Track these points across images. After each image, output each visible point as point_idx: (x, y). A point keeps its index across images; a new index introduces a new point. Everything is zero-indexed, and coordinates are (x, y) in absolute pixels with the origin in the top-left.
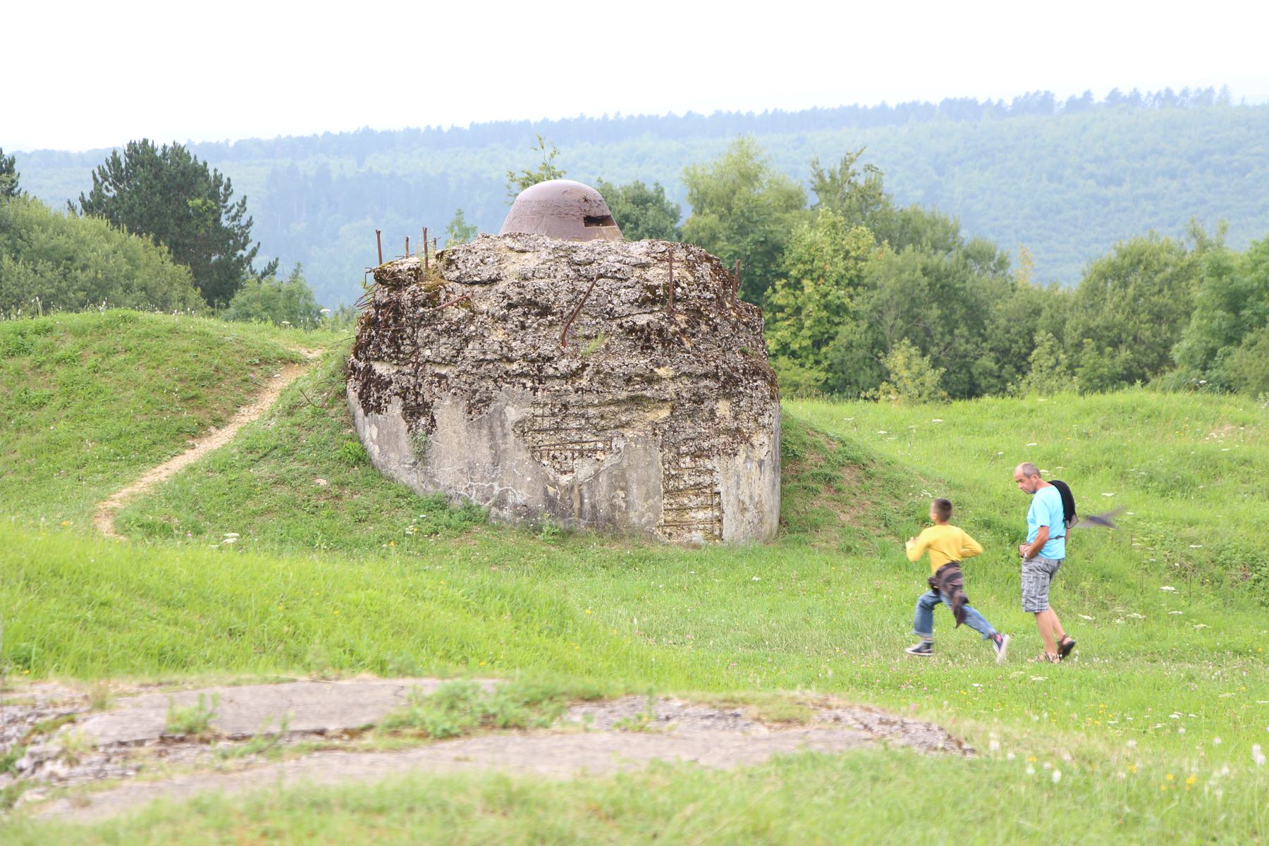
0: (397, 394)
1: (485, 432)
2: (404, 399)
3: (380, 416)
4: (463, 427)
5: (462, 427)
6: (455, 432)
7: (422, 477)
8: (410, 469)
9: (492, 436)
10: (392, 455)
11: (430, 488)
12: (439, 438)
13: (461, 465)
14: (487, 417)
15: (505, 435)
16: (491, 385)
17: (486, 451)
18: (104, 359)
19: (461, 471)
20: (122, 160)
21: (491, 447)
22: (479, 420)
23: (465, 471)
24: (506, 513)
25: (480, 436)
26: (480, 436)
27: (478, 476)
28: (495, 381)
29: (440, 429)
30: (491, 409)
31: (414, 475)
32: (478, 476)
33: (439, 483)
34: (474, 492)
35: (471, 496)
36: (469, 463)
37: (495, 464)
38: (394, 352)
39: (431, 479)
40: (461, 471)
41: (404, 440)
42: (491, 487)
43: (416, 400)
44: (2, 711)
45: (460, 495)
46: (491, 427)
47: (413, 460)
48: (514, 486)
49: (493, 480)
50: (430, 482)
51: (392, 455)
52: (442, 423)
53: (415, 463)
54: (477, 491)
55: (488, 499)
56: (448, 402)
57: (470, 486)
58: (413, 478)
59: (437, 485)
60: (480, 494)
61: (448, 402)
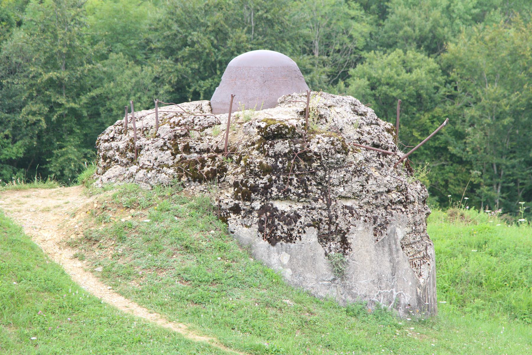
0: (309, 225)
1: (386, 249)
2: (319, 229)
3: (292, 245)
4: (373, 247)
5: (372, 246)
6: (367, 252)
7: (341, 290)
8: (329, 285)
9: (391, 254)
10: (308, 275)
11: (349, 298)
12: (355, 257)
13: (374, 277)
14: (387, 237)
15: (398, 250)
16: (382, 211)
17: (388, 264)
18: (468, 95)
19: (373, 282)
20: (36, 178)
21: (390, 261)
22: (383, 240)
23: (376, 281)
24: (401, 312)
25: (383, 253)
26: (383, 253)
27: (384, 285)
28: (386, 208)
29: (354, 251)
30: (389, 231)
31: (335, 290)
32: (384, 285)
33: (356, 294)
34: (382, 298)
35: (380, 301)
36: (378, 275)
37: (393, 274)
38: (303, 192)
39: (350, 291)
40: (373, 282)
41: (323, 264)
42: (392, 292)
43: (329, 229)
44: (1, 24)
45: (373, 301)
46: (390, 245)
47: (332, 277)
48: (404, 291)
49: (393, 287)
50: (348, 293)
51: (308, 275)
52: (357, 245)
53: (334, 280)
54: (384, 297)
55: (390, 302)
56: (360, 228)
57: (380, 294)
58: (332, 292)
59: (354, 296)
60: (385, 299)
61: (360, 228)
